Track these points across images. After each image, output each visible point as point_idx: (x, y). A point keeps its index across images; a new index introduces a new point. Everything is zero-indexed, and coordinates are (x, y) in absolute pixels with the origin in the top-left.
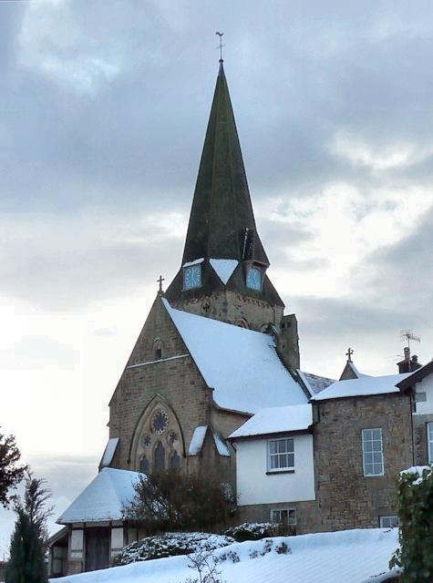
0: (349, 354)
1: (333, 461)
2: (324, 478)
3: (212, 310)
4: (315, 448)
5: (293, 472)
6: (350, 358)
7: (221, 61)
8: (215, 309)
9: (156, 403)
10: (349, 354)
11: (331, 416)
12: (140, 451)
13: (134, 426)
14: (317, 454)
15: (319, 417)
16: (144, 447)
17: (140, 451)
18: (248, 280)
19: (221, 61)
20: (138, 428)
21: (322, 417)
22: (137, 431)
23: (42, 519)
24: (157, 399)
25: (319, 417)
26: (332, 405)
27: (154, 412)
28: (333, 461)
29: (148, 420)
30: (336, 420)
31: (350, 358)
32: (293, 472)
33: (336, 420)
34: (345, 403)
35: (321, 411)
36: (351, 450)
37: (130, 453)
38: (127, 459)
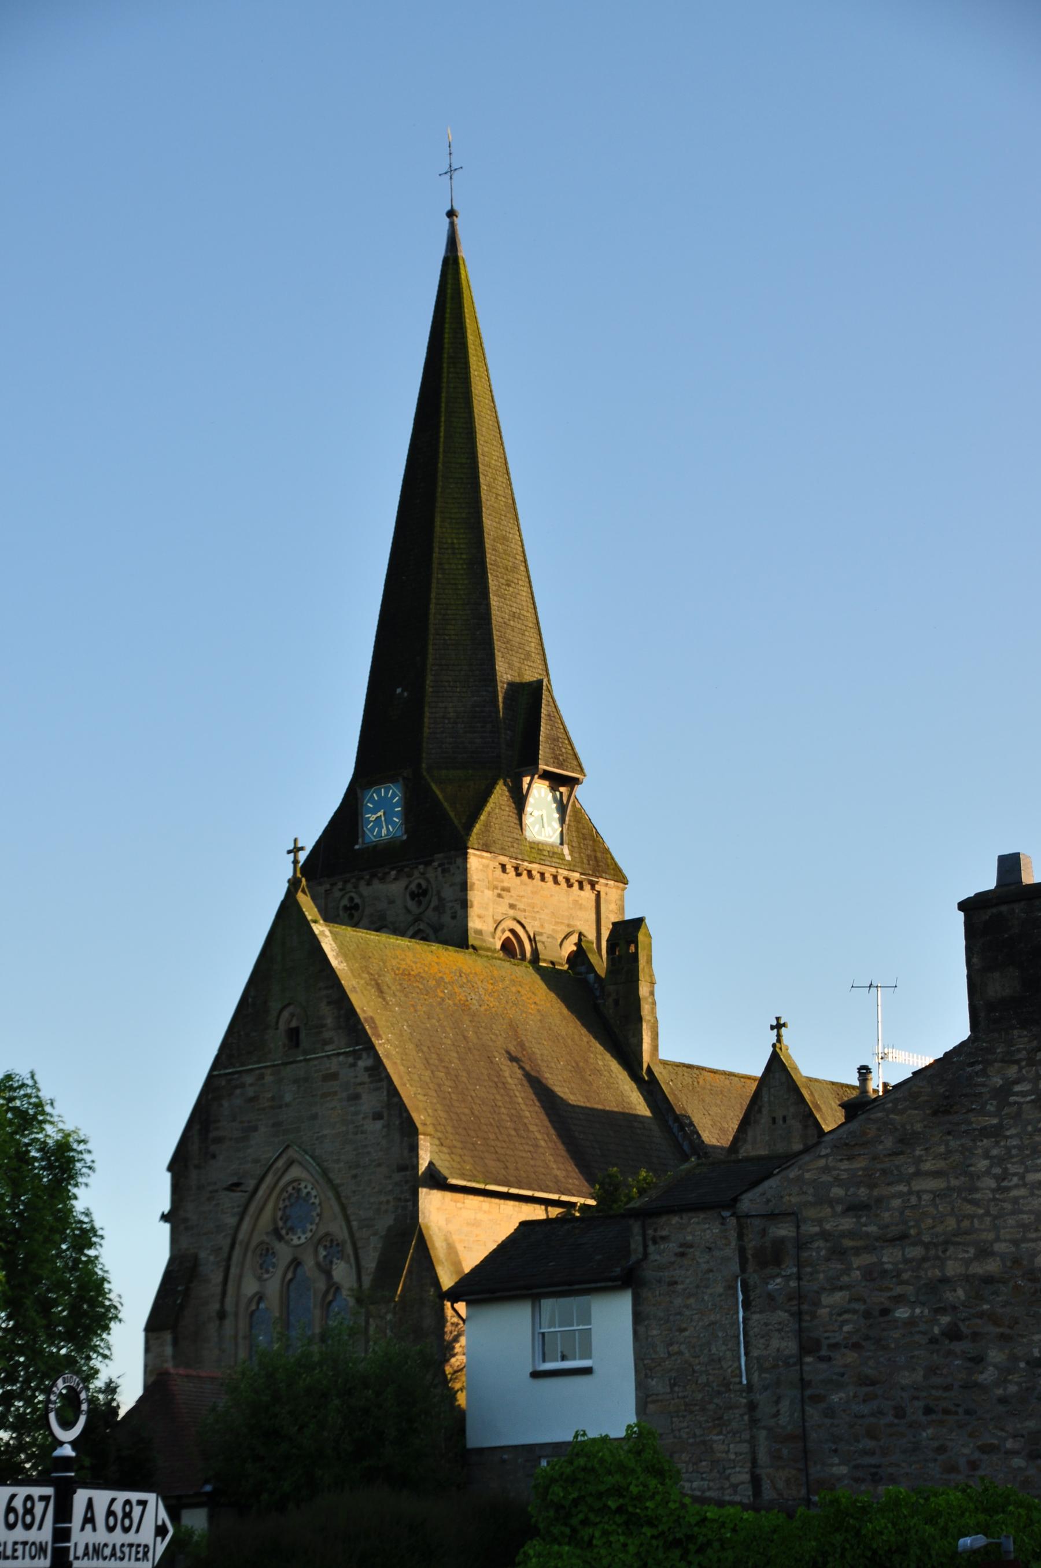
0: (779, 1026)
1: (675, 1348)
2: (655, 1384)
3: (435, 902)
4: (638, 1318)
5: (587, 1371)
6: (779, 1036)
7: (451, 214)
8: (441, 899)
9: (290, 1163)
10: (779, 1026)
11: (673, 1246)
12: (250, 1287)
13: (232, 1221)
14: (641, 1329)
15: (645, 1246)
16: (260, 1279)
17: (250, 1287)
18: (528, 820)
19: (451, 214)
20: (246, 1226)
21: (651, 1248)
22: (242, 1236)
23: (81, 1174)
24: (291, 1153)
25: (645, 1246)
26: (675, 1220)
27: (284, 1189)
28: (675, 1348)
29: (270, 1205)
30: (682, 1255)
31: (779, 1036)
32: (587, 1371)
33: (682, 1255)
34: (702, 1216)
35: (650, 1232)
36: (713, 1323)
37: (224, 1293)
38: (216, 1306)
